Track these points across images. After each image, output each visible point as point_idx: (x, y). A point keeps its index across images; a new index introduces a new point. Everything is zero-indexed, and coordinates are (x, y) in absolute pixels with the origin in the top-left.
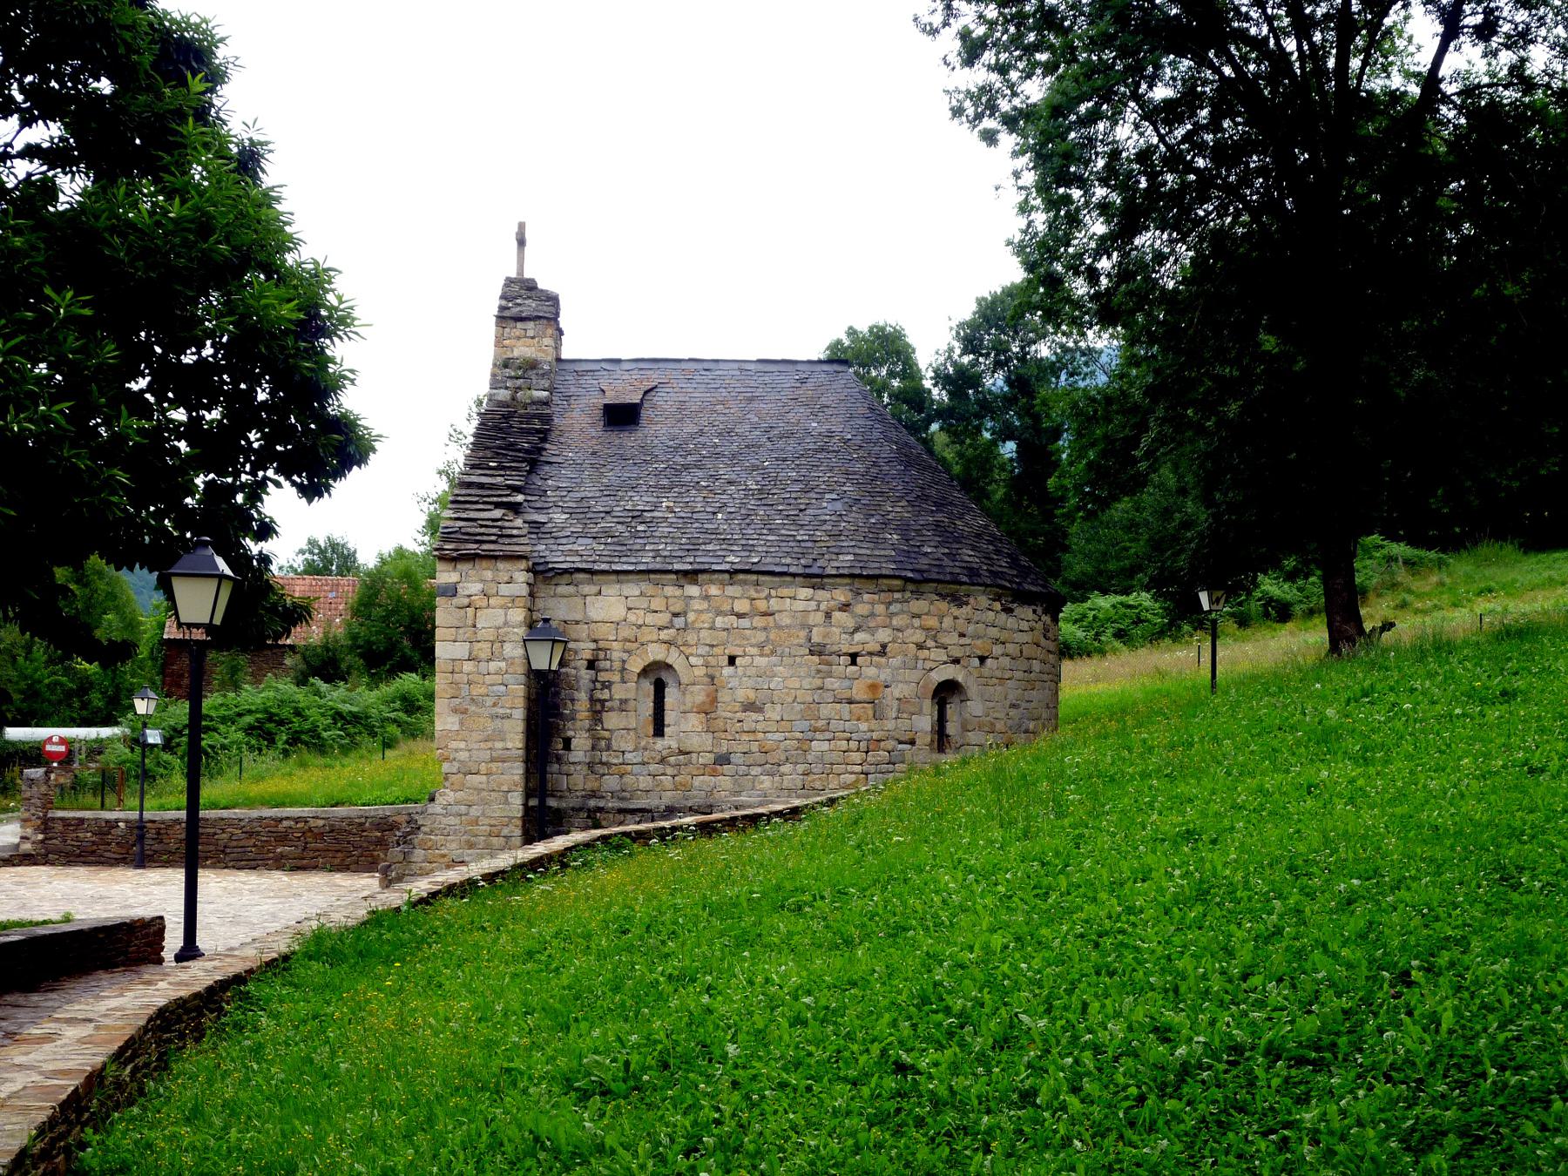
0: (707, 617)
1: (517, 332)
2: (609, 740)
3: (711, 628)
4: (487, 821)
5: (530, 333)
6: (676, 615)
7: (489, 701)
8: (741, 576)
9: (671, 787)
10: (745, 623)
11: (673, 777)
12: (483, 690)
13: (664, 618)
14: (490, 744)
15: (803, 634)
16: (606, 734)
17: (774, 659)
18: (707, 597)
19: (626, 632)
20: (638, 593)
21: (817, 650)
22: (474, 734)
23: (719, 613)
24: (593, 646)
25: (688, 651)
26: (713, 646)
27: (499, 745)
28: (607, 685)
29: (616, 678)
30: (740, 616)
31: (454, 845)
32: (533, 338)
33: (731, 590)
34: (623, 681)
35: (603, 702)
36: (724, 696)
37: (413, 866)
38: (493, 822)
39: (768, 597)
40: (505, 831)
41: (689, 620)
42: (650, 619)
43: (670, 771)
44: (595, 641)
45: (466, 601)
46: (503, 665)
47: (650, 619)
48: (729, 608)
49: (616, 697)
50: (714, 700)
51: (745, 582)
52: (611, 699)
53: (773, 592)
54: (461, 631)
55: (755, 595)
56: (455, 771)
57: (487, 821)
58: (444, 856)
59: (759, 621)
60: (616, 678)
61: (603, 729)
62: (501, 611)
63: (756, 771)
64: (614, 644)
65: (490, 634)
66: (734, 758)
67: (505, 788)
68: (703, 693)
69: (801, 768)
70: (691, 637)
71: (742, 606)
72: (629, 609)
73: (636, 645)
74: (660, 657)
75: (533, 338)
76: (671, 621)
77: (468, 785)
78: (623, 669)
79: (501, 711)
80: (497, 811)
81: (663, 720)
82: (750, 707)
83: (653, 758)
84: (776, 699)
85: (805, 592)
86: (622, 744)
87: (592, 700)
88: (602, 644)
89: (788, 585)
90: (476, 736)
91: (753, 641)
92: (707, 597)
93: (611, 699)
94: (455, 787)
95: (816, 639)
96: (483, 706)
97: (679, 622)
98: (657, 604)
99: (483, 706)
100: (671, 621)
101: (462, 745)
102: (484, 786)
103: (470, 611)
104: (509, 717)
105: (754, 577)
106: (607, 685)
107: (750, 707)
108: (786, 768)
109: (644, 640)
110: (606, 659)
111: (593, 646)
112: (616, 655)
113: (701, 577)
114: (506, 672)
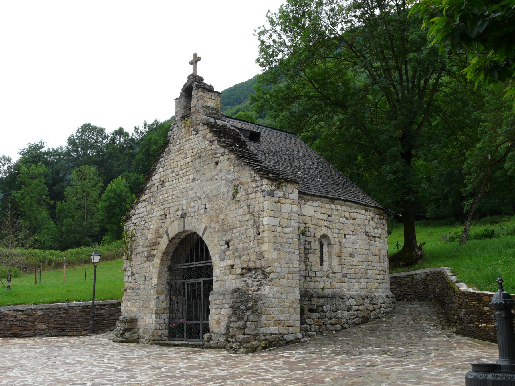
0: (337, 217)
1: (209, 96)
2: (311, 266)
3: (339, 223)
4: (288, 301)
5: (213, 98)
6: (329, 216)
7: (287, 245)
8: (347, 203)
9: (330, 287)
10: (348, 221)
11: (331, 283)
12: (285, 241)
13: (325, 217)
14: (288, 265)
15: (364, 228)
16: (310, 264)
17: (357, 237)
18: (337, 210)
19: (315, 221)
20: (317, 205)
21: (367, 235)
22: (282, 260)
23: (341, 217)
24: (304, 226)
25: (333, 231)
26: (340, 230)
27: (291, 266)
28: (310, 243)
29: (312, 240)
30: (347, 219)
31: (277, 313)
32: (214, 100)
33: (344, 208)
34: (314, 242)
35: (309, 250)
36: (344, 250)
37: (262, 323)
38: (290, 301)
39: (354, 212)
40: (294, 306)
41: (333, 218)
42: (321, 216)
43: (330, 280)
44: (305, 224)
45: (277, 199)
46: (291, 229)
47: (321, 216)
48: (343, 215)
49: (313, 248)
50: (341, 252)
51: (347, 206)
52: (311, 249)
53: (355, 211)
54: (276, 213)
55: (351, 211)
56: (276, 277)
57: (288, 301)
58: (273, 317)
59: (352, 221)
60: (312, 240)
61: (309, 262)
62: (290, 206)
63: (354, 281)
64: (311, 225)
65: (286, 215)
66: (349, 276)
67: (294, 286)
68: (338, 249)
69: (366, 280)
70: (334, 225)
71: (347, 215)
72: (315, 211)
73: (318, 227)
74: (325, 232)
75: (214, 100)
76: (328, 218)
77: (281, 284)
78: (315, 236)
79: (291, 250)
80: (291, 296)
81: (323, 259)
82: (351, 255)
83: (325, 275)
84: (358, 253)
85: (363, 212)
86: (315, 268)
87: (305, 249)
88: (307, 225)
89: (358, 208)
90: (283, 261)
91: (351, 229)
92: (337, 210)
93: (311, 249)
94: (277, 285)
95: (367, 230)
96: (285, 248)
97: (330, 218)
98: (323, 211)
99: (285, 248)
100: (328, 218)
101: (278, 265)
102: (286, 284)
103: (279, 204)
104: (294, 253)
105: (350, 204)
106: (310, 243)
107: (351, 255)
108: (362, 280)
109: (321, 225)
110: (309, 232)
111: (304, 226)
112: (312, 230)
113: (337, 201)
114: (293, 233)
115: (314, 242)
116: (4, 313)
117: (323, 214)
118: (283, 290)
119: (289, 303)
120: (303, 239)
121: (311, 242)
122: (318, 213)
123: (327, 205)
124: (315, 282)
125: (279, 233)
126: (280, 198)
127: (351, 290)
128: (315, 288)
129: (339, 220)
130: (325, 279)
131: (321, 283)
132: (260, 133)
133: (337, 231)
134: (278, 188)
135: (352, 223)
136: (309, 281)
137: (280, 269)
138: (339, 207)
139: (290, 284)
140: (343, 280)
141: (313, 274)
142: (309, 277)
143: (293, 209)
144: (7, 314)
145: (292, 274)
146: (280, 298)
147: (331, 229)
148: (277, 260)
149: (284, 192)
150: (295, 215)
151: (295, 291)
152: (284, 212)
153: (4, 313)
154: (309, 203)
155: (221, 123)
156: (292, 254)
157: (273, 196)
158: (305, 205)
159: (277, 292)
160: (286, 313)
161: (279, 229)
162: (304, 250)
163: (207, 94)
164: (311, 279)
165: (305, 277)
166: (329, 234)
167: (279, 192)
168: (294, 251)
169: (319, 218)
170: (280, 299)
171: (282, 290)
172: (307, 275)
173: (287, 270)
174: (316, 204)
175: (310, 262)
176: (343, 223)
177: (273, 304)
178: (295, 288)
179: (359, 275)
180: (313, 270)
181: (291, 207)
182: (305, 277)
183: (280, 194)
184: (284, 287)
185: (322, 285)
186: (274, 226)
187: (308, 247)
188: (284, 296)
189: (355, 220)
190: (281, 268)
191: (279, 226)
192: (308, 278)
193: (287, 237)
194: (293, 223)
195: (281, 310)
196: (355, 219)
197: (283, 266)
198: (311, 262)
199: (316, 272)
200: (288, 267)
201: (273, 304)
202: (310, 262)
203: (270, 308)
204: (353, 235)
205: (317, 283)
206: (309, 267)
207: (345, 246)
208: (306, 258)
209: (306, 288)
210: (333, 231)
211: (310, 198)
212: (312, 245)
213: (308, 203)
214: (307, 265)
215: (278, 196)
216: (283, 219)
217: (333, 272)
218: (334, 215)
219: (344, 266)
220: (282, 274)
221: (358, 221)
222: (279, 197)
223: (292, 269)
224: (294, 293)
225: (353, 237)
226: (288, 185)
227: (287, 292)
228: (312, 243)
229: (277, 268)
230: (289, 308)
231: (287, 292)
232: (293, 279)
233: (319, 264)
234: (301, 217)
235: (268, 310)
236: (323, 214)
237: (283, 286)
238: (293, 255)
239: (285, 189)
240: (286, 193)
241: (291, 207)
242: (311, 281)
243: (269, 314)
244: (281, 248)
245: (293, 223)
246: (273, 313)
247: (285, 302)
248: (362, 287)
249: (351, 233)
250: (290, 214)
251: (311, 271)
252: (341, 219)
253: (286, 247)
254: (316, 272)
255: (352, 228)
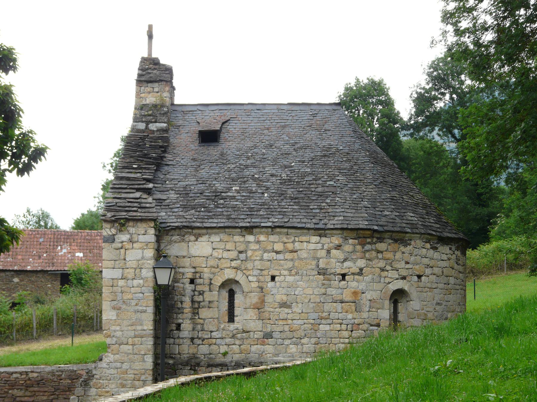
2: (203, 324)
4: (132, 372)
5: (156, 90)
6: (240, 252)
7: (133, 303)
8: (278, 230)
10: (280, 256)
11: (240, 345)
12: (130, 296)
13: (234, 254)
14: (134, 327)
15: (314, 263)
18: (258, 242)
19: (211, 263)
20: (218, 240)
21: (322, 272)
22: (124, 322)
23: (265, 251)
25: (248, 273)
26: (262, 270)
27: (139, 328)
28: (201, 293)
30: (277, 252)
33: (272, 238)
35: (199, 302)
36: (269, 299)
38: (136, 372)
39: (294, 242)
41: (248, 255)
42: (226, 255)
43: (237, 342)
44: (194, 268)
45: (120, 245)
47: (226, 255)
48: (271, 248)
49: (207, 299)
50: (263, 301)
52: (204, 301)
53: (297, 239)
54: (117, 262)
55: (286, 240)
57: (132, 372)
59: (288, 256)
60: (206, 288)
61: (199, 318)
62: (140, 251)
63: (287, 342)
64: (205, 269)
65: (134, 264)
66: (275, 335)
67: (143, 353)
68: (257, 297)
69: (313, 340)
70: (249, 265)
71: (278, 247)
72: (214, 249)
73: (218, 270)
74: (231, 276)
76: (238, 256)
78: (211, 284)
79: (141, 308)
80: (138, 366)
82: (284, 305)
83: (228, 335)
87: (193, 302)
88: (198, 269)
90: (126, 323)
91: (286, 267)
92: (258, 242)
93: (204, 301)
94: (114, 352)
95: (321, 265)
97: (243, 256)
98: (229, 246)
101: (118, 328)
102: (131, 351)
103: (122, 251)
104: (145, 311)
105: (286, 230)
106: (201, 293)
110: (200, 278)
112: (206, 276)
115: (210, 290)
116: (77, 372)
117: (229, 250)
118: (126, 359)
119: (135, 374)
120: (190, 288)
121: (204, 292)
122: (219, 250)
123: (237, 238)
124: (210, 345)
125: (121, 287)
126: (124, 243)
127: (280, 355)
128: (210, 354)
129: (262, 256)
130: (228, 340)
131: (221, 346)
132: (200, 132)
133: (256, 272)
134: (121, 231)
135: (289, 258)
136: (199, 345)
137: (121, 333)
138: (262, 238)
139: (136, 351)
140: (264, 342)
141: (207, 334)
142: (200, 339)
143: (144, 254)
144: (80, 374)
145: (140, 339)
146: (120, 368)
147: (244, 271)
148: (115, 322)
149: (131, 235)
150: (148, 262)
151: (146, 359)
152: (130, 260)
153: (77, 372)
154: (205, 238)
155: (156, 127)
156: (141, 312)
157: (113, 242)
158: (196, 243)
159: (115, 361)
160: (129, 386)
161: (121, 283)
162: (190, 303)
163: (145, 87)
164: (203, 341)
165: (192, 339)
166: (239, 277)
167: (122, 236)
168: (144, 308)
169: (220, 257)
170: (119, 370)
171: (123, 358)
172: (196, 337)
173: (132, 334)
174: (215, 238)
175: (201, 319)
176: (269, 261)
177: (108, 376)
178: (145, 356)
179: (301, 333)
180: (206, 329)
181: (143, 253)
182: (192, 339)
183: (124, 237)
184: (126, 355)
185: (223, 349)
186: (113, 279)
187: (197, 298)
188: (126, 365)
189: (295, 254)
190: (122, 331)
191: (122, 279)
192: (196, 341)
193: (133, 292)
194: (144, 273)
195: (121, 384)
196: (296, 252)
197: (126, 329)
198: (204, 319)
199: (211, 332)
200: (134, 330)
201: (108, 376)
202: (201, 319)
203: (103, 380)
204: (290, 275)
205: (214, 347)
206: (199, 327)
207: (272, 293)
208: (194, 313)
209: (193, 354)
210: (248, 273)
211: (204, 231)
212: (205, 296)
213: (200, 239)
214: (195, 324)
215: (120, 241)
216: (128, 270)
217: (244, 331)
218: (251, 250)
219: (268, 322)
220: (123, 339)
221: (304, 254)
222: (122, 242)
223: (140, 332)
224: (144, 361)
225: (290, 279)
226: (138, 224)
227: (132, 361)
228: (205, 293)
229: (115, 331)
230: (134, 380)
231: (132, 361)
232: (141, 344)
233: (226, 319)
234: (189, 259)
235: (100, 383)
236: (229, 250)
237: (125, 353)
238: (143, 314)
239: (132, 230)
240: (134, 236)
241: (143, 253)
242: (202, 344)
243: (102, 387)
244: (124, 306)
245: (144, 273)
246: (107, 387)
247: (127, 374)
248: (305, 350)
249: (286, 273)
250: (139, 262)
251: (202, 331)
252: (266, 255)
253: (132, 304)
254: (211, 332)
255: (290, 264)
